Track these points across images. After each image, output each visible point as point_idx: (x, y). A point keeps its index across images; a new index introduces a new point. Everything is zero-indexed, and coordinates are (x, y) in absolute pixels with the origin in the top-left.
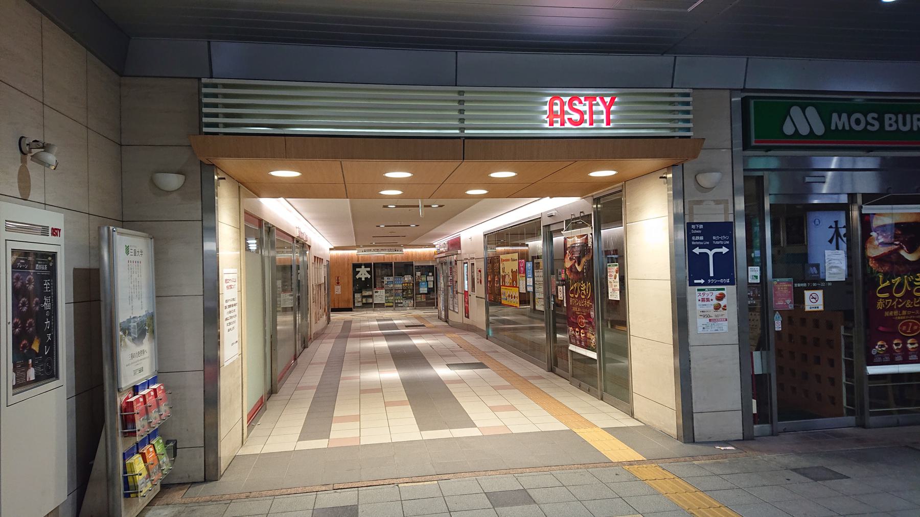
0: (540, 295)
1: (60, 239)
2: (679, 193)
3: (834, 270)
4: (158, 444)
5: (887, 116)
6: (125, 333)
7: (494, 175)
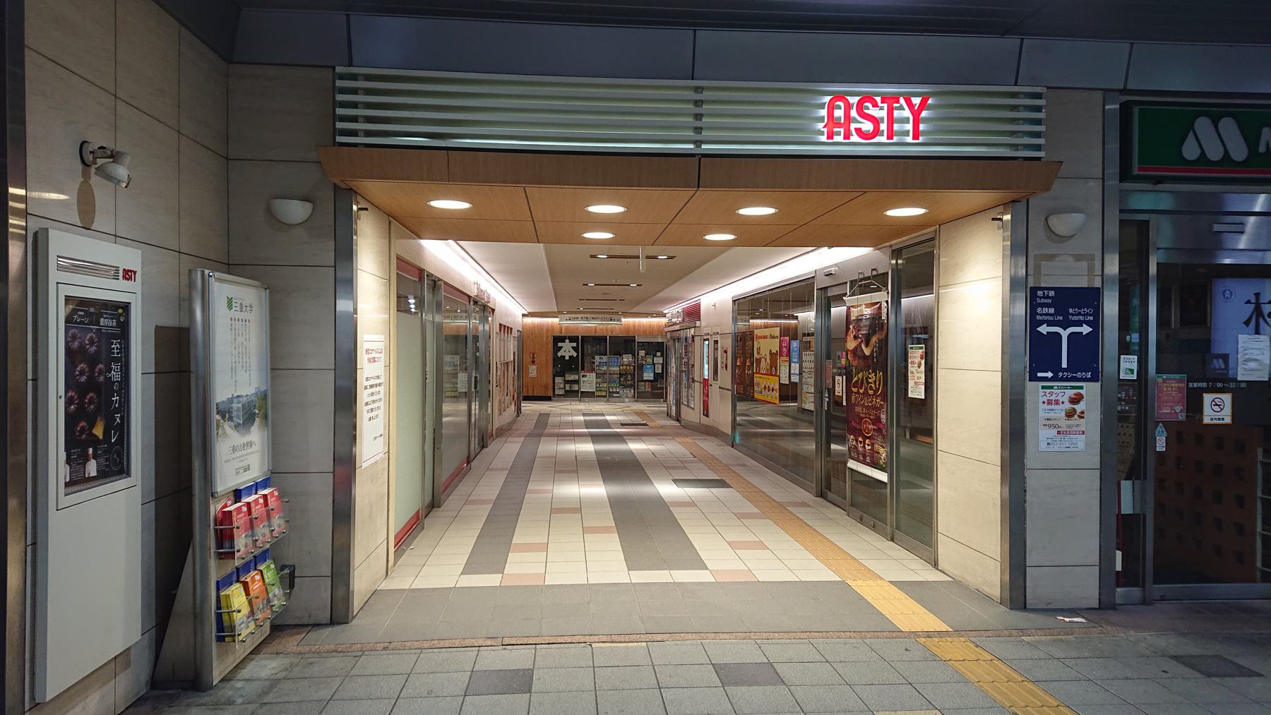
0: (809, 388)
1: (136, 286)
2: (1019, 248)
3: (1252, 365)
4: (269, 571)
6: (223, 417)
7: (743, 212)
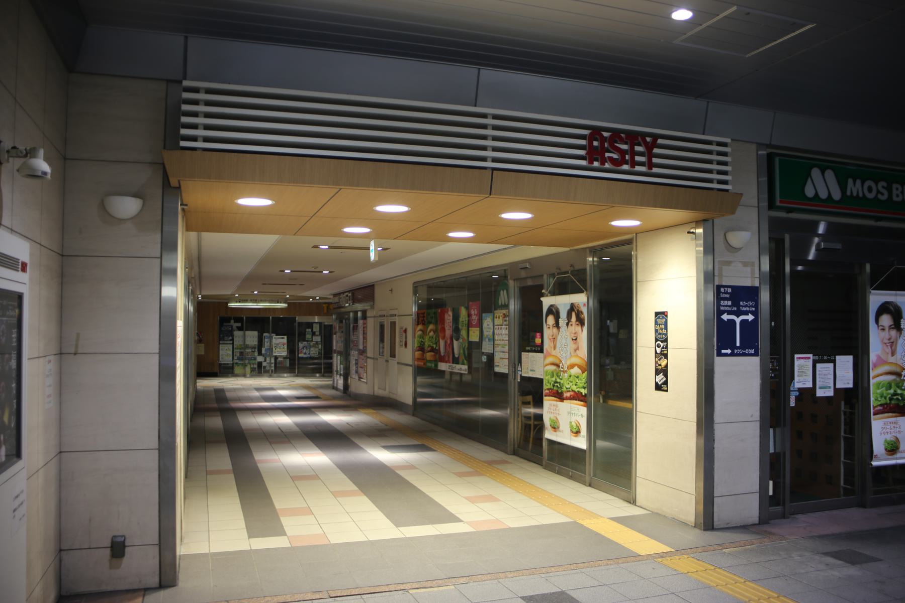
2: (709, 249)
5: (895, 186)
